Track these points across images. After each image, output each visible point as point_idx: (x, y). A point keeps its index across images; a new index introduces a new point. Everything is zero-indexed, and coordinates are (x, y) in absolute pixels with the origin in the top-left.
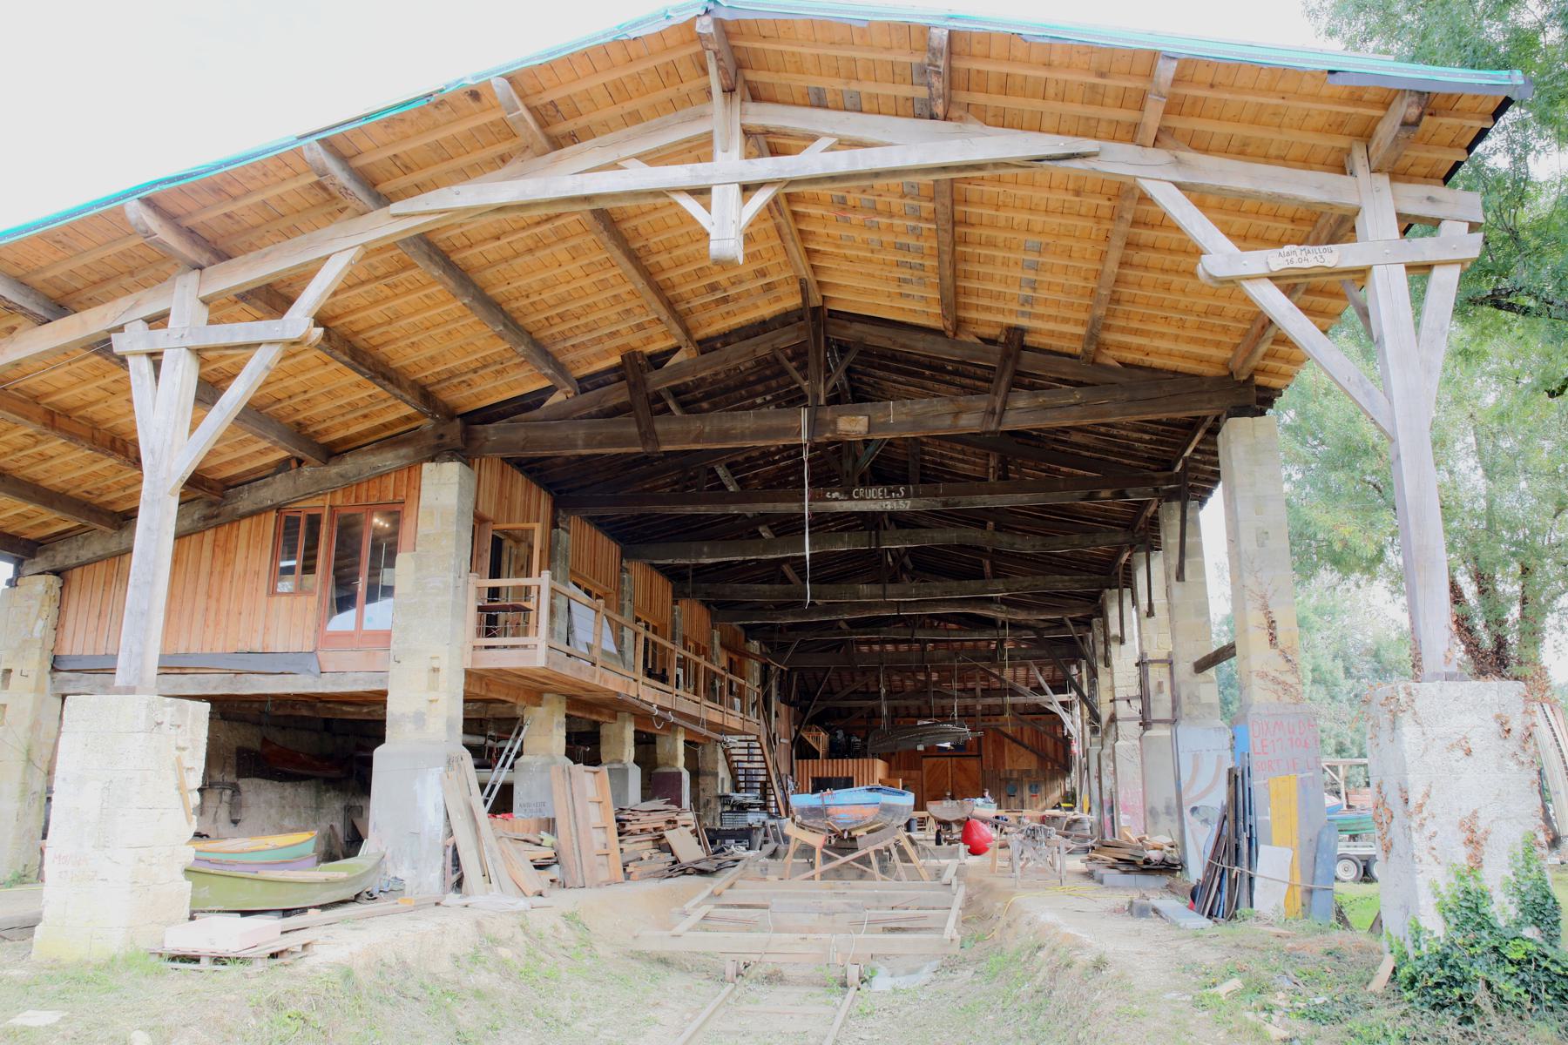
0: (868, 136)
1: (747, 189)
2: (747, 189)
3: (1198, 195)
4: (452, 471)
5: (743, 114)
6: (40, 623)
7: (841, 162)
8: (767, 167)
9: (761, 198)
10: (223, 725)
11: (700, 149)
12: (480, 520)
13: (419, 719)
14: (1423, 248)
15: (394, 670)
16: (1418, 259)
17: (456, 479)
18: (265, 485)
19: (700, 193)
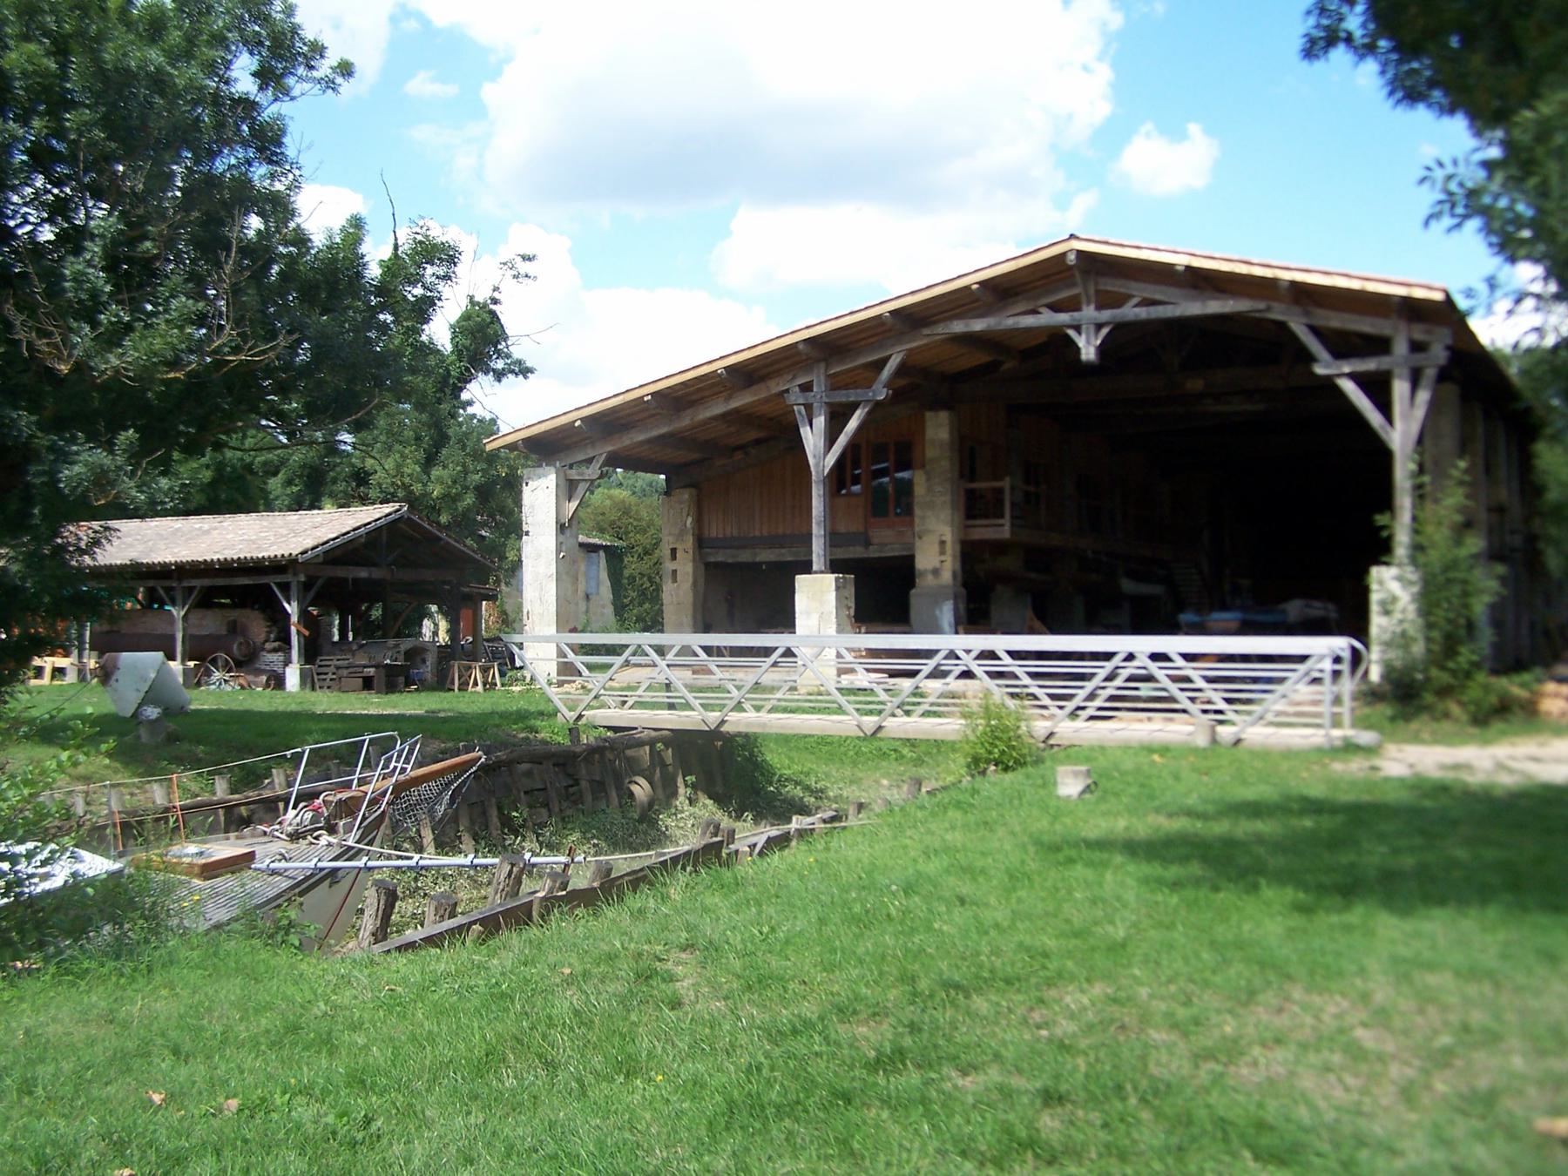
0: (1158, 297)
1: (1099, 327)
2: (1099, 327)
3: (1316, 331)
4: (943, 417)
5: (1096, 283)
6: (690, 520)
7: (1143, 313)
8: (1106, 315)
9: (1105, 331)
10: (995, 613)
11: (1072, 305)
12: (1102, 748)
13: (936, 572)
14: (1419, 358)
15: (918, 543)
16: (968, 682)
17: (947, 422)
18: (1149, 719)
19: (1078, 329)
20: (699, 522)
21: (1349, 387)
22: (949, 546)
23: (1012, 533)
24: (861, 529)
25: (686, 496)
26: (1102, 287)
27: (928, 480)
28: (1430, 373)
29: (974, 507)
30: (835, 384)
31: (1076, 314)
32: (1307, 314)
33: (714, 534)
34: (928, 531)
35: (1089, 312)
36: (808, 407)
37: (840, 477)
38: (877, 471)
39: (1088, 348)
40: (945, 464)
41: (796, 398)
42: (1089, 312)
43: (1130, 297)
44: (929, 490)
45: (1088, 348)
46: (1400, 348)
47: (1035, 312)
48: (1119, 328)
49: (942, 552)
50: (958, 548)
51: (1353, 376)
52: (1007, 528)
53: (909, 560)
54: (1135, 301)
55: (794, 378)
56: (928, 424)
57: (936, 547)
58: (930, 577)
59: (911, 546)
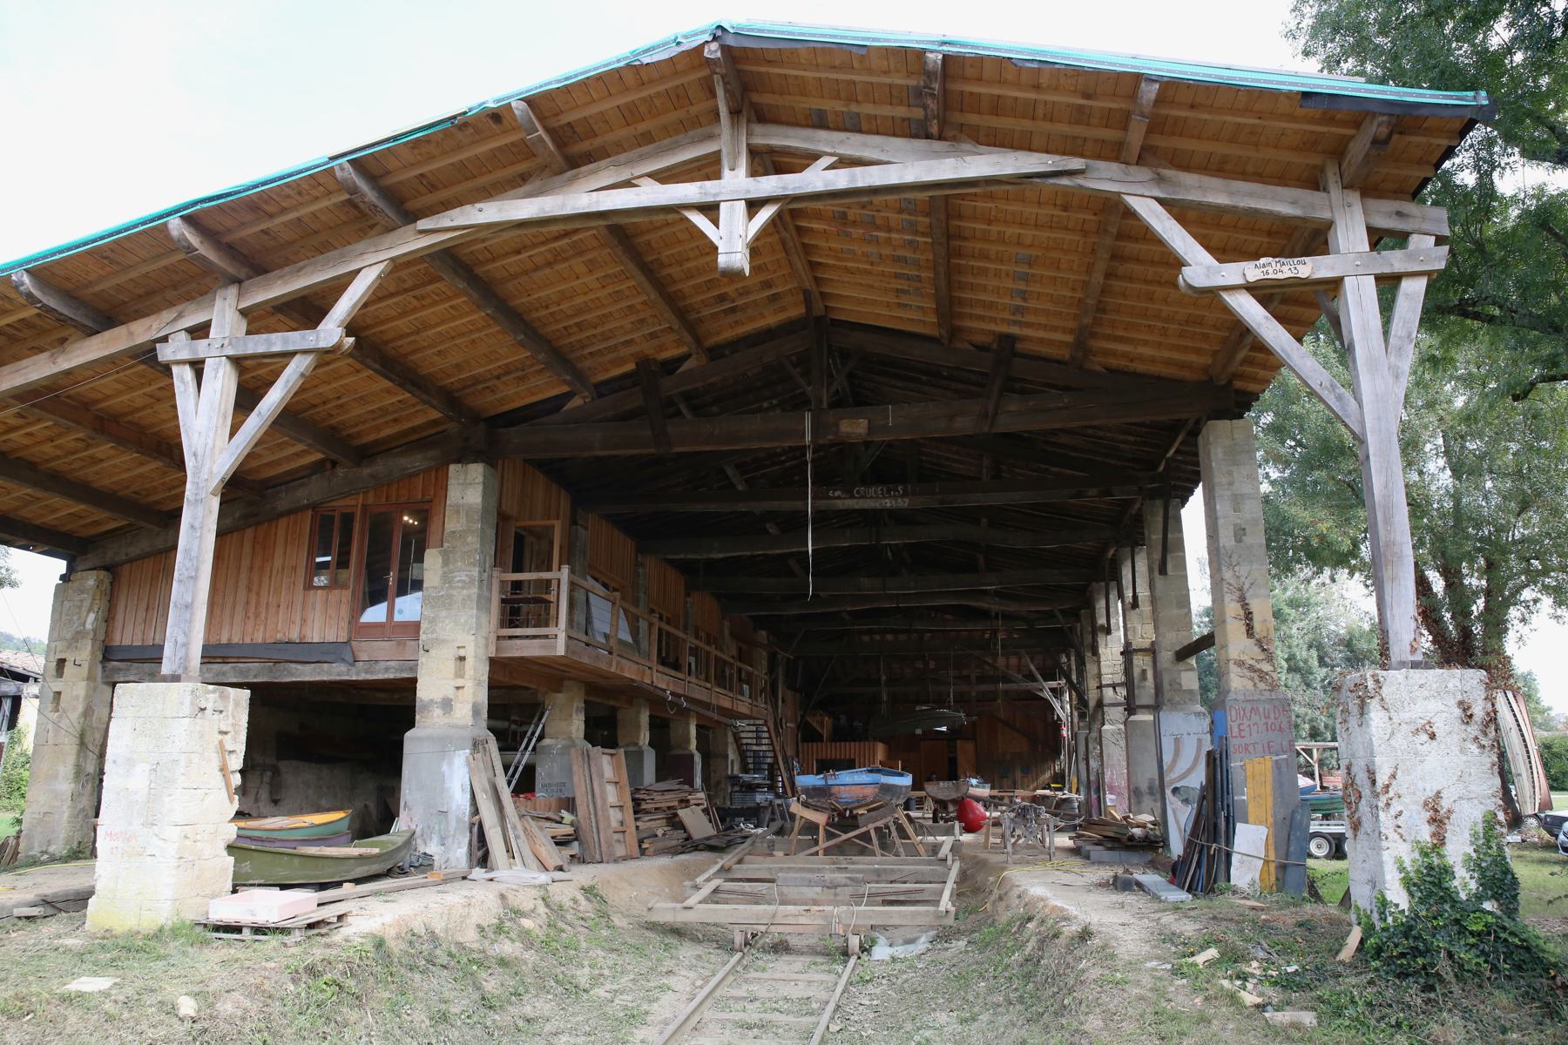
0: (867, 154)
1: (753, 206)
2: (753, 206)
4: (476, 471)
6: (92, 616)
7: (842, 179)
8: (771, 185)
9: (765, 214)
11: (708, 168)
13: (447, 705)
14: (1394, 261)
15: (423, 659)
17: (480, 479)
20: (108, 619)
21: (1250, 310)
22: (470, 662)
23: (567, 647)
24: (343, 638)
25: (91, 582)
26: (758, 141)
27: (446, 563)
28: (1413, 293)
29: (519, 609)
30: (256, 320)
31: (709, 185)
32: (1160, 180)
33: (127, 642)
34: (440, 642)
35: (736, 182)
36: (197, 366)
37: (245, 495)
38: (332, 497)
39: (733, 240)
40: (473, 541)
41: (176, 349)
42: (736, 182)
43: (815, 157)
44: (447, 579)
45: (733, 240)
46: (1351, 235)
47: (628, 184)
48: (793, 211)
49: (460, 674)
50: (484, 670)
51: (1251, 288)
52: (562, 637)
53: (408, 687)
54: (826, 161)
55: (180, 316)
56: (452, 482)
57: (450, 666)
58: (437, 712)
59: (413, 665)
